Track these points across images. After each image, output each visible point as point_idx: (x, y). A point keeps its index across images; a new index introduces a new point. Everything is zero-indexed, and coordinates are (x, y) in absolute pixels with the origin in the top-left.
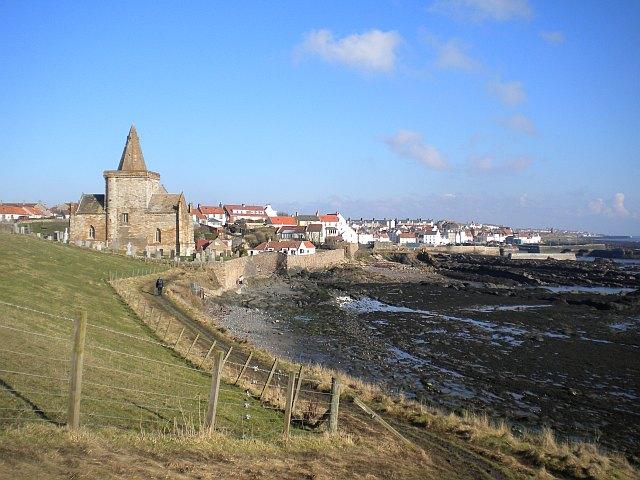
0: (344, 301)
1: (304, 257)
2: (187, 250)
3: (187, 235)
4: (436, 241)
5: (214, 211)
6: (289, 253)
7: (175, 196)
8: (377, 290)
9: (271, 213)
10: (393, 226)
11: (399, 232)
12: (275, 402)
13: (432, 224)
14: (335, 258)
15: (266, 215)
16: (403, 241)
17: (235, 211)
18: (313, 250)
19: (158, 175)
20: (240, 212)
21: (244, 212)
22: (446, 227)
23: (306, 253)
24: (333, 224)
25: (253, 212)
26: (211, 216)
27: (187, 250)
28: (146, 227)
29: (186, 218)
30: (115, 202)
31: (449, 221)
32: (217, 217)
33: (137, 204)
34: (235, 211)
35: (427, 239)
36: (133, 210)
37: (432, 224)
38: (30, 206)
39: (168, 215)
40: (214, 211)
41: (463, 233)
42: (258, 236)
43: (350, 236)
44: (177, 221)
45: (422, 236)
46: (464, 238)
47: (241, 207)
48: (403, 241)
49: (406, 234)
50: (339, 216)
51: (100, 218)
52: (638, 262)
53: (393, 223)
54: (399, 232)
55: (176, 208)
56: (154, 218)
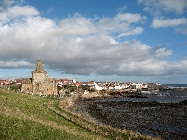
0: (100, 107)
1: (86, 94)
2: (56, 94)
3: (56, 89)
4: (119, 88)
5: (59, 81)
6: (82, 93)
7: (52, 78)
8: (111, 104)
9: (75, 82)
10: (106, 84)
11: (108, 86)
12: (178, 119)
13: (117, 83)
14: (93, 95)
15: (73, 82)
16: (110, 88)
17: (64, 81)
18: (88, 92)
19: (47, 72)
20: (66, 81)
21: (67, 81)
22: (121, 84)
23: (86, 93)
24: (92, 84)
25: (69, 81)
26: (58, 83)
27: (56, 94)
28: (44, 87)
29: (55, 84)
30: (35, 80)
31: (122, 82)
32: (60, 83)
33: (41, 81)
34: (64, 81)
35: (116, 87)
36: (40, 82)
37: (117, 83)
38: (5, 80)
39: (50, 84)
40: (59, 81)
41: (126, 85)
42: (72, 89)
43: (98, 88)
44: (53, 85)
45: (115, 87)
46: (126, 87)
47: (66, 80)
48: (110, 88)
49: (110, 86)
50: (94, 82)
51: (30, 85)
52: (186, 129)
53: (106, 83)
54: (108, 86)
55: (53, 81)
56: (46, 84)
